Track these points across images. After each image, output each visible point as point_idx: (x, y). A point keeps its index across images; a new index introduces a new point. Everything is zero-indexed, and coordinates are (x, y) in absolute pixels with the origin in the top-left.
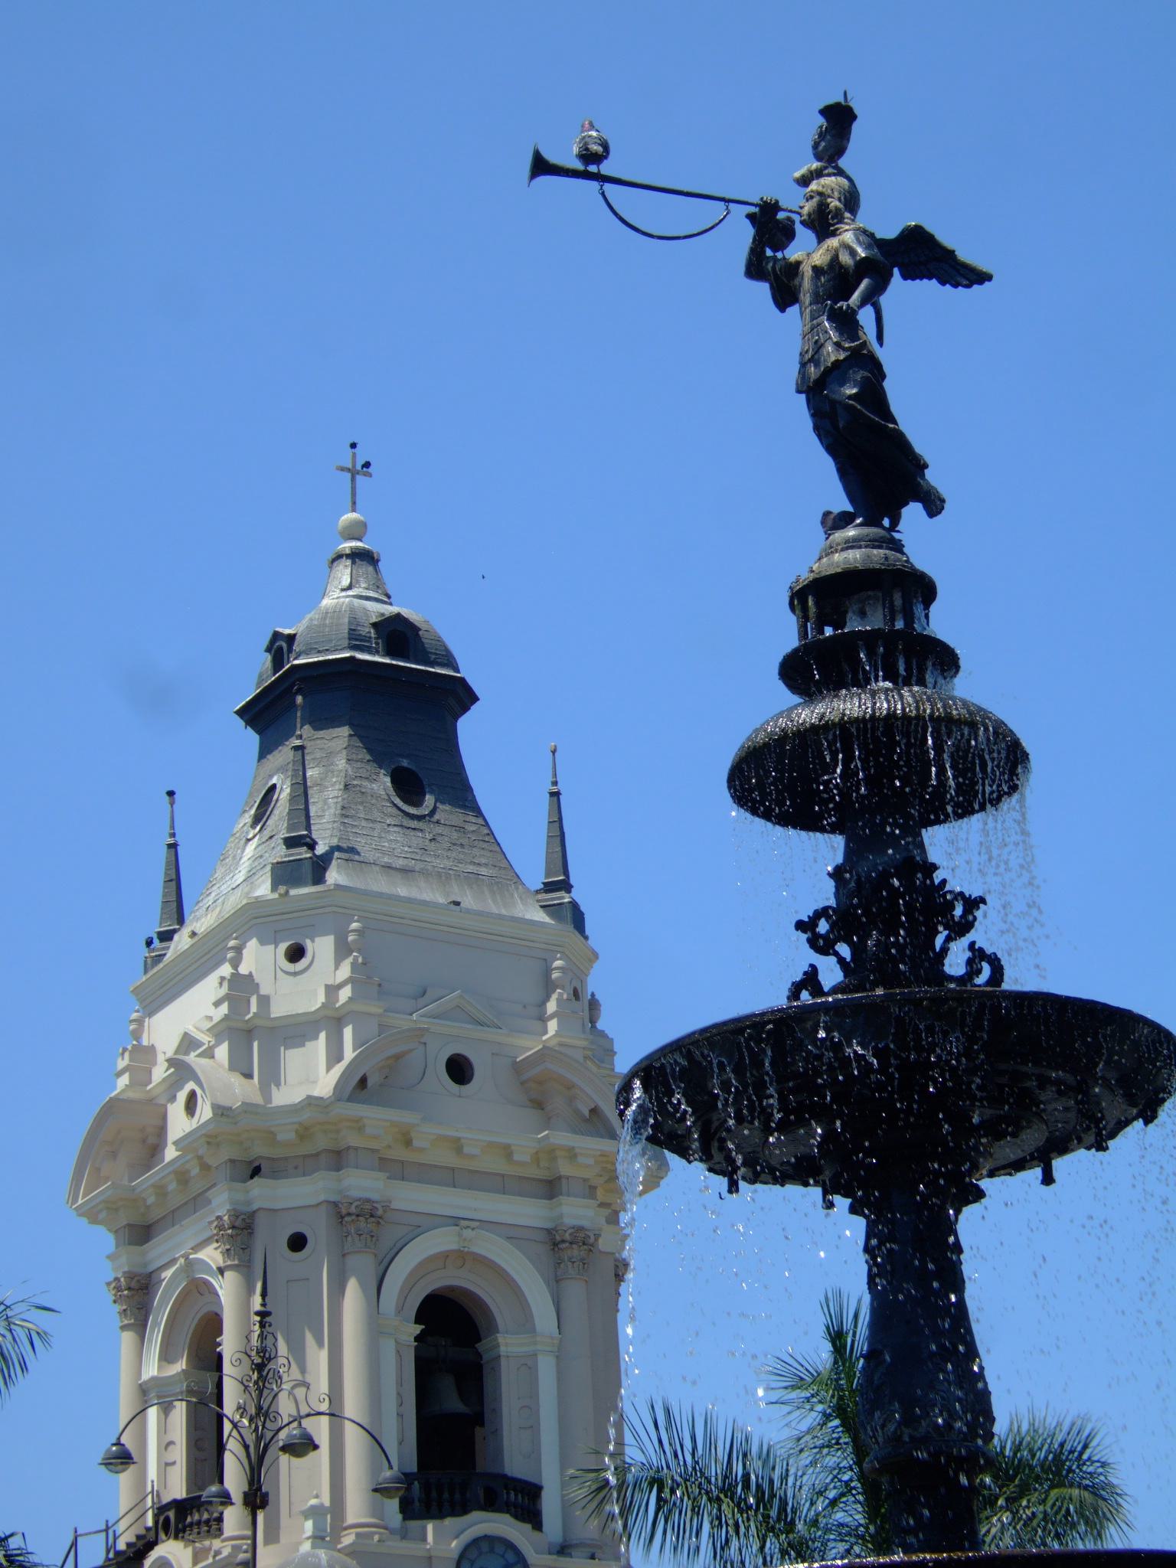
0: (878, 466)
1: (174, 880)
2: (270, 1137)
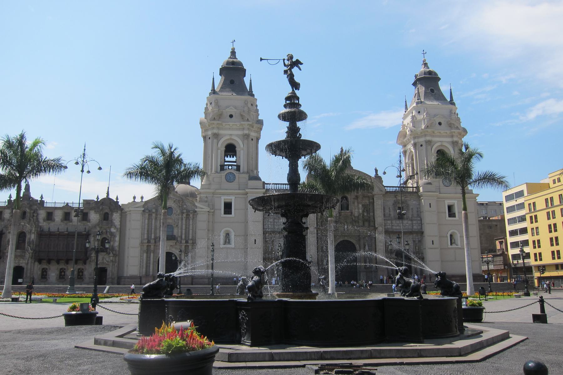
0: (295, 85)
2: (417, 134)
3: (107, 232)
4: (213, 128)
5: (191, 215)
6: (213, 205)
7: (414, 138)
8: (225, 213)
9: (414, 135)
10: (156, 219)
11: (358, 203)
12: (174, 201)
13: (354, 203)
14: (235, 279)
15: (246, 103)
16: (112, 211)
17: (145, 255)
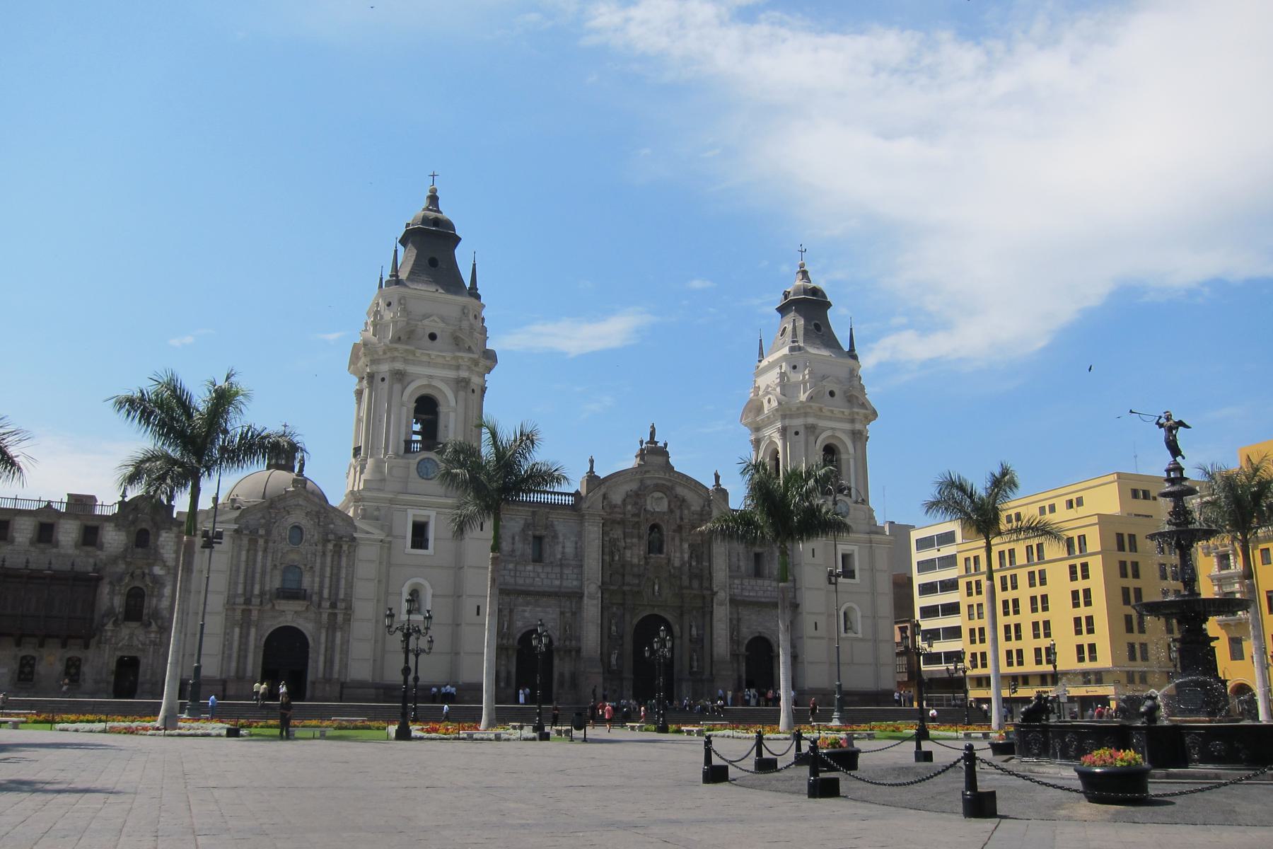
0: (1174, 450)
1: (761, 348)
3: (144, 574)
4: (393, 359)
5: (345, 547)
6: (391, 528)
7: (784, 417)
8: (413, 546)
9: (784, 412)
10: (265, 550)
11: (681, 540)
12: (307, 514)
13: (673, 539)
14: (434, 690)
15: (464, 310)
16: (158, 528)
17: (237, 630)
